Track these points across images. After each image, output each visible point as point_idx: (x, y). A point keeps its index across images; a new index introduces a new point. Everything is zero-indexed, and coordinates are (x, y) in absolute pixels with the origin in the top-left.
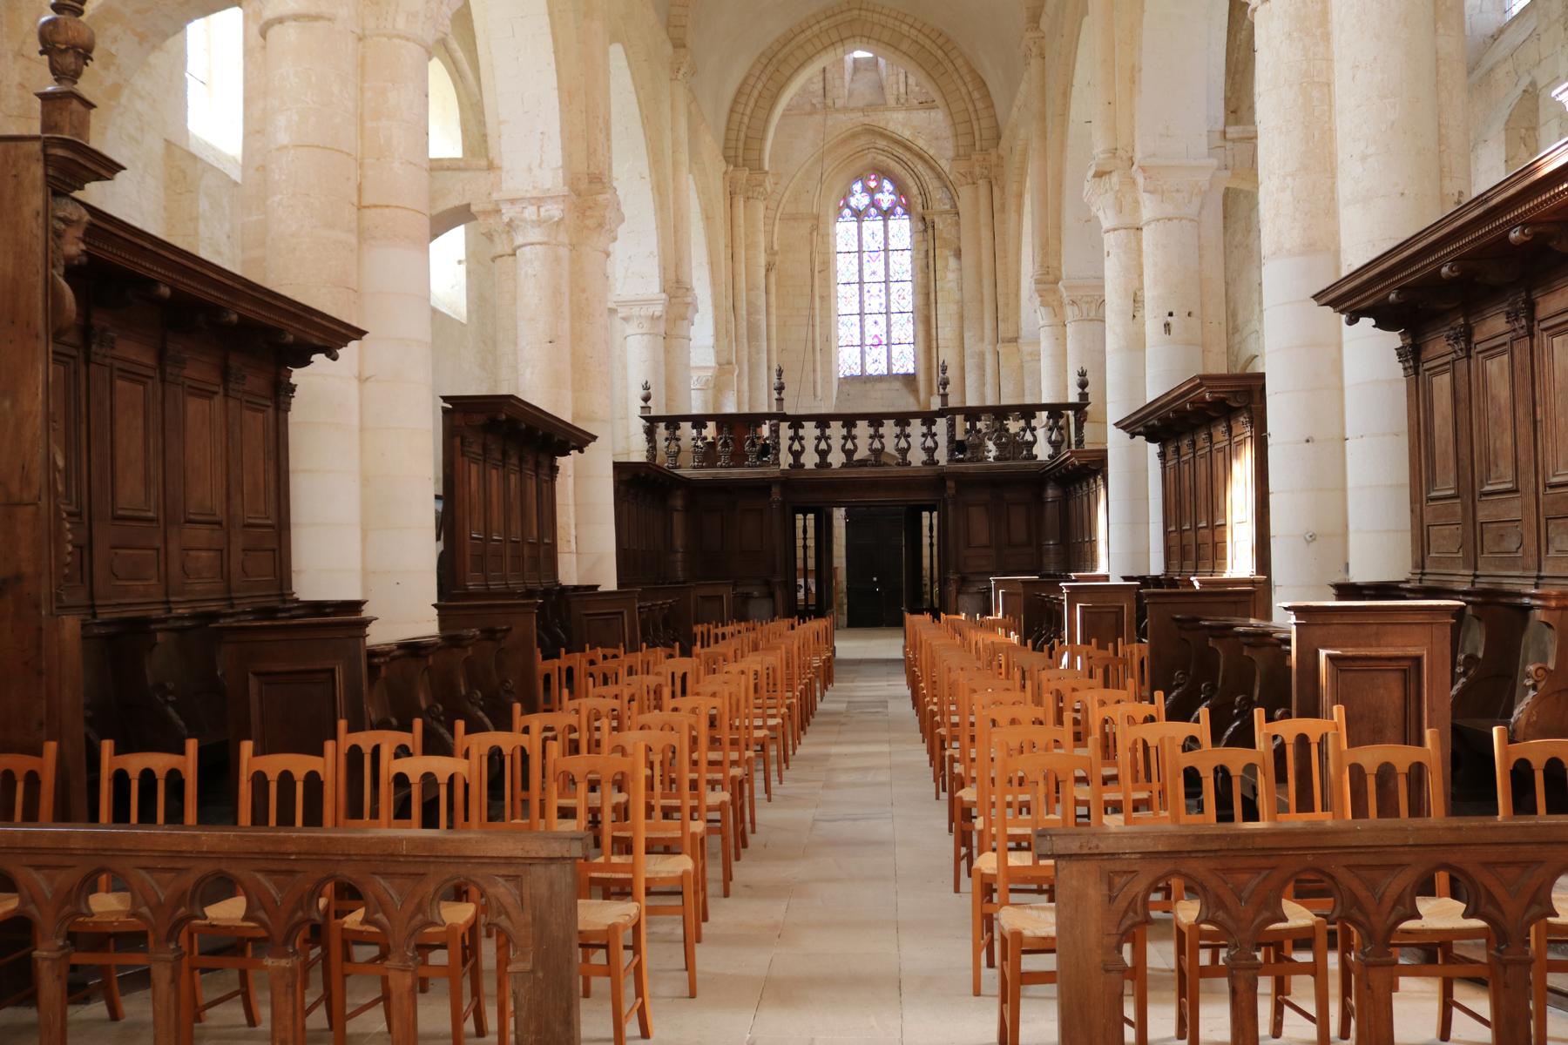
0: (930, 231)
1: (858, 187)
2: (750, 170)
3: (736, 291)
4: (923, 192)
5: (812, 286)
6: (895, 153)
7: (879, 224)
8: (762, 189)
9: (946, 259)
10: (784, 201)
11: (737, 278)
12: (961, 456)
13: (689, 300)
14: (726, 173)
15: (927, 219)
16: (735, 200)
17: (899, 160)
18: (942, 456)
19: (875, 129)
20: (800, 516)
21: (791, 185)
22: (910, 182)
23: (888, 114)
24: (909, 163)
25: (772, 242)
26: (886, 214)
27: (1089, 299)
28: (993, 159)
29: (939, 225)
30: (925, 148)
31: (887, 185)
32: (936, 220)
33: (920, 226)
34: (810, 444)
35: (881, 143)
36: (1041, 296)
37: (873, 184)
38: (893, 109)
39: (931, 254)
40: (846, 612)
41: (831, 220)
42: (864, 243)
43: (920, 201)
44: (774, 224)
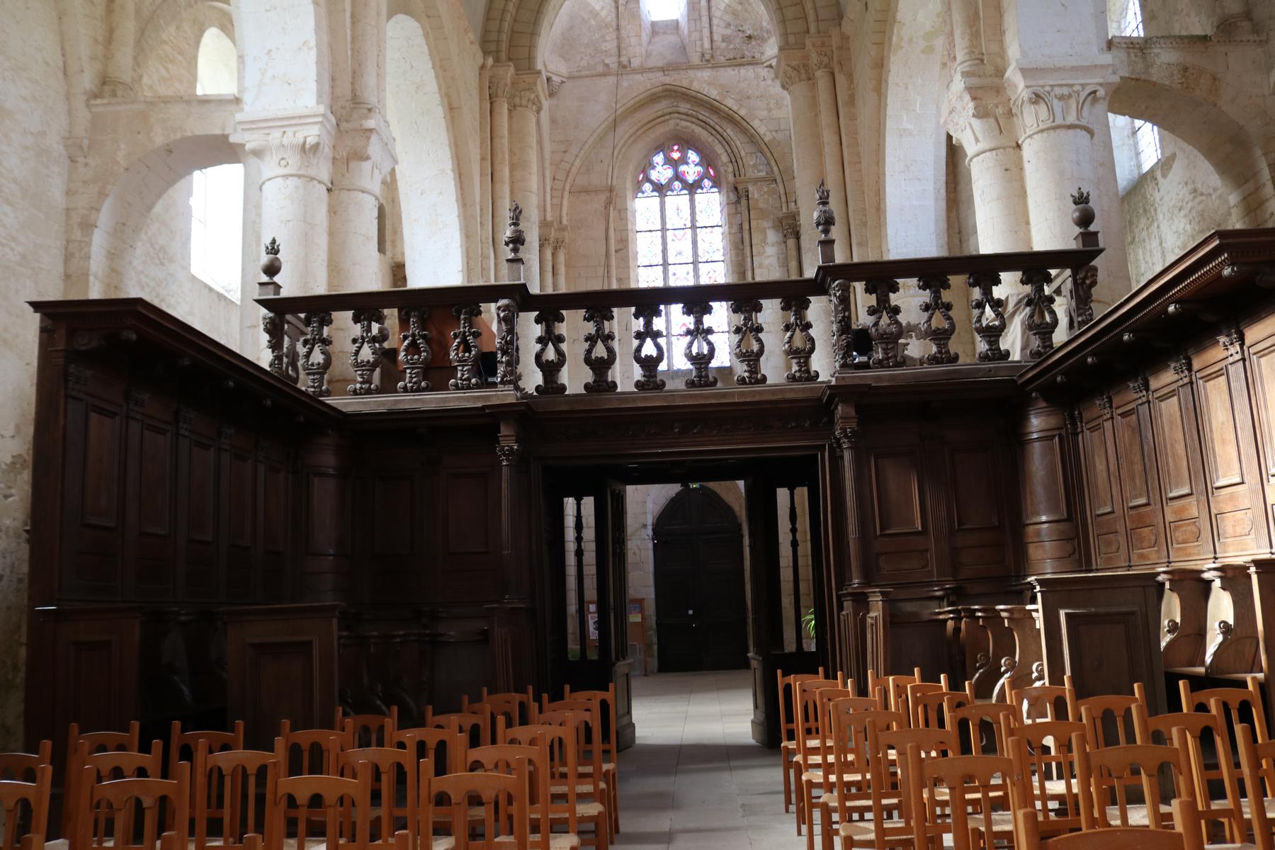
0: (744, 202)
1: (659, 159)
2: (517, 69)
3: (497, 220)
4: (735, 159)
5: (607, 239)
6: (701, 117)
7: (684, 199)
8: (533, 96)
9: (764, 231)
10: (574, 170)
11: (498, 203)
12: (864, 359)
13: (371, 123)
14: (483, 67)
15: (740, 187)
16: (496, 105)
17: (705, 125)
18: (824, 364)
19: (679, 89)
20: (570, 503)
21: (582, 152)
22: (719, 149)
23: (692, 73)
24: (718, 128)
25: (561, 217)
26: (692, 188)
27: (1065, 91)
28: (835, 41)
29: (754, 192)
30: (735, 108)
31: (693, 156)
32: (750, 188)
33: (733, 197)
34: (574, 348)
35: (684, 107)
36: (974, 99)
37: (676, 155)
38: (697, 68)
39: (746, 226)
40: (656, 654)
41: (629, 194)
42: (667, 220)
43: (730, 169)
44: (562, 198)
